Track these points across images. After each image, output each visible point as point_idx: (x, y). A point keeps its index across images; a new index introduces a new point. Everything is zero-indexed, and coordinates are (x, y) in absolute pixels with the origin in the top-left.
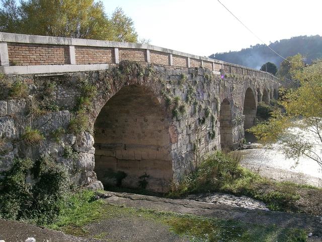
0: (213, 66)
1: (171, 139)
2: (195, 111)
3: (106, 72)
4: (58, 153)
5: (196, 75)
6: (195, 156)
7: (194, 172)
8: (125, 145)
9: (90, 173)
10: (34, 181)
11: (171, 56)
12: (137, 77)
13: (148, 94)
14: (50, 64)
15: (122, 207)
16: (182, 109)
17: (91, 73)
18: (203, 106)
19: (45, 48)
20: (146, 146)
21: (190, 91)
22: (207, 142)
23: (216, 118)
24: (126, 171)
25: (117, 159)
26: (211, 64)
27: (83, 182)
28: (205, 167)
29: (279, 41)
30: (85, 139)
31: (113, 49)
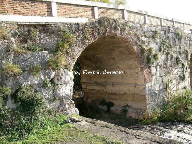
0: (184, 26)
1: (145, 79)
2: (167, 59)
3: (86, 24)
4: (38, 84)
5: (168, 33)
6: (167, 93)
7: (165, 105)
9: (69, 102)
10: (14, 105)
12: (115, 30)
13: (126, 44)
15: (83, 131)
16: (155, 57)
17: (71, 25)
18: (175, 56)
19: (28, 3)
20: (127, 84)
21: (163, 43)
22: (178, 83)
23: (186, 64)
24: (114, 102)
25: (108, 93)
26: (182, 25)
27: (61, 108)
28: (175, 102)
30: (64, 74)
31: (93, 7)
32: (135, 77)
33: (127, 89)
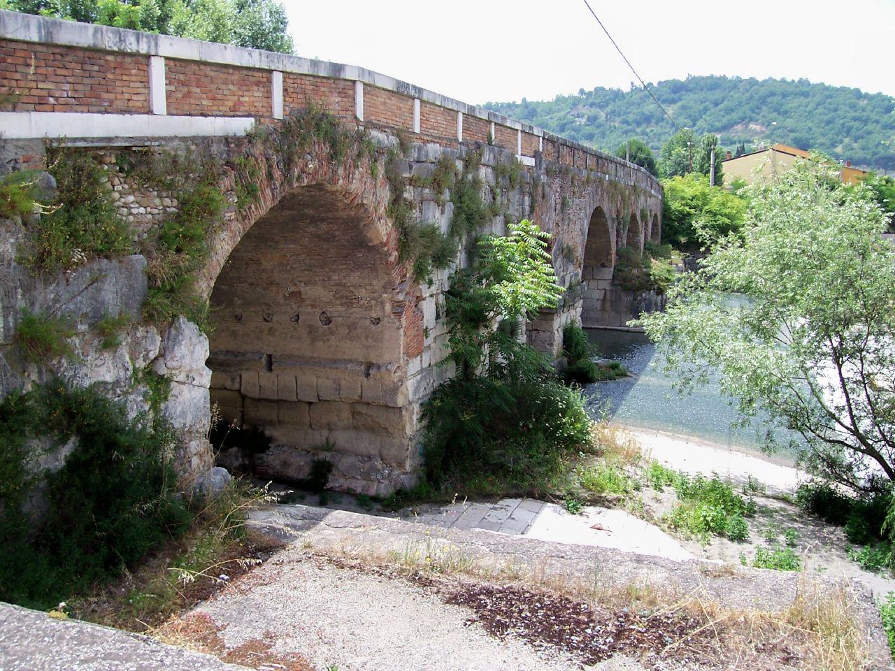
8: (270, 357)
11: (417, 103)
14: (95, 108)
25: (244, 397)
29: (655, 85)
32: (367, 337)
33: (329, 383)
